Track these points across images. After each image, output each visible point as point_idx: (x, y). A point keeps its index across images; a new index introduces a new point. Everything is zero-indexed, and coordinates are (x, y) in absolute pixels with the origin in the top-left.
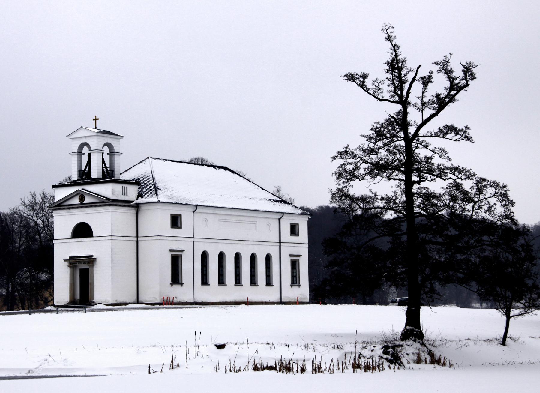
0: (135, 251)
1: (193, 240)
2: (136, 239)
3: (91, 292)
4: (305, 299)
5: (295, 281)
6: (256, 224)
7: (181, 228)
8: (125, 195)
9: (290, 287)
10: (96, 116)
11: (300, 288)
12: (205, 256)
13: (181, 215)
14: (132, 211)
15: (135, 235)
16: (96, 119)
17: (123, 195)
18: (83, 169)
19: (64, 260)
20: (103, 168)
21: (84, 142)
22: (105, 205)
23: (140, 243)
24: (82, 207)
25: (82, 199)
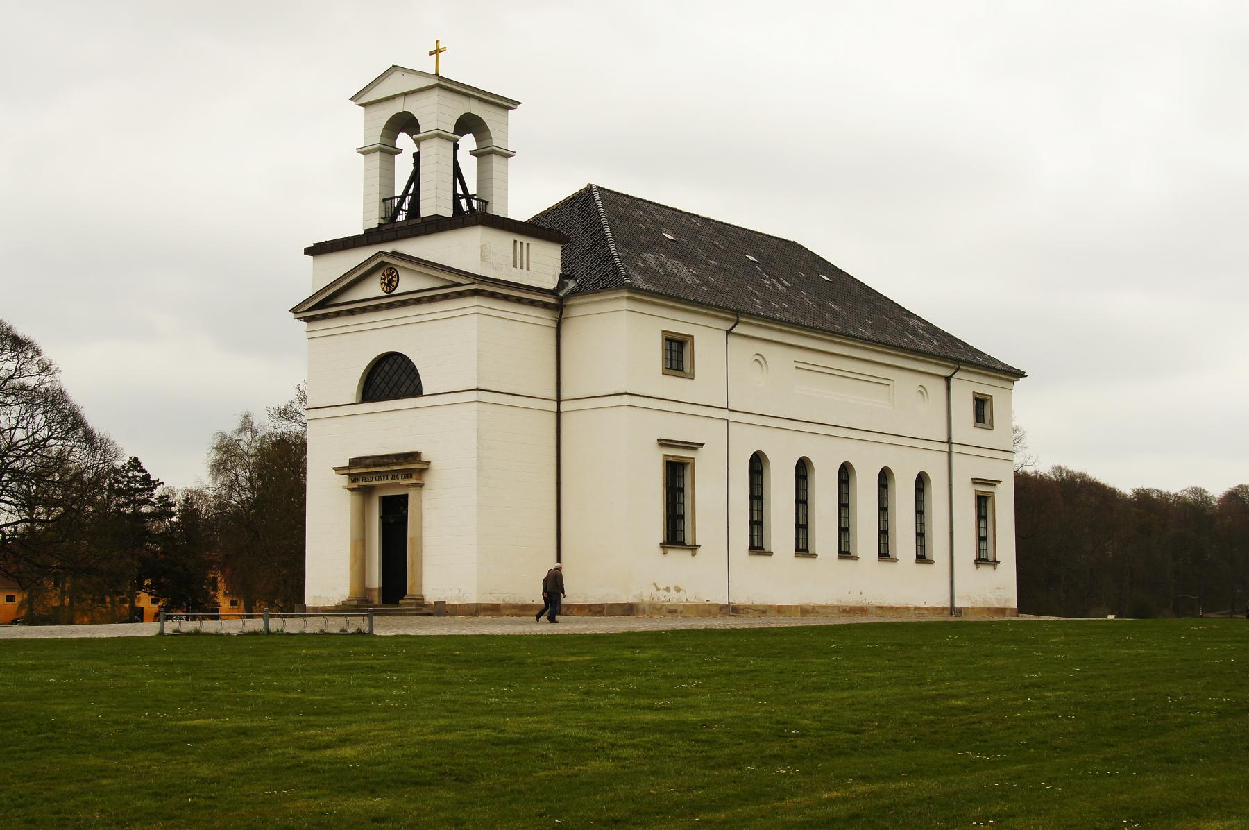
1: (725, 414)
2: (554, 406)
4: (1007, 600)
5: (984, 559)
7: (691, 376)
8: (522, 268)
11: (996, 570)
12: (757, 464)
13: (692, 337)
14: (540, 320)
15: (553, 395)
16: (437, 52)
17: (515, 266)
18: (399, 191)
20: (455, 194)
22: (461, 295)
23: (563, 416)
24: (390, 306)
25: (390, 284)
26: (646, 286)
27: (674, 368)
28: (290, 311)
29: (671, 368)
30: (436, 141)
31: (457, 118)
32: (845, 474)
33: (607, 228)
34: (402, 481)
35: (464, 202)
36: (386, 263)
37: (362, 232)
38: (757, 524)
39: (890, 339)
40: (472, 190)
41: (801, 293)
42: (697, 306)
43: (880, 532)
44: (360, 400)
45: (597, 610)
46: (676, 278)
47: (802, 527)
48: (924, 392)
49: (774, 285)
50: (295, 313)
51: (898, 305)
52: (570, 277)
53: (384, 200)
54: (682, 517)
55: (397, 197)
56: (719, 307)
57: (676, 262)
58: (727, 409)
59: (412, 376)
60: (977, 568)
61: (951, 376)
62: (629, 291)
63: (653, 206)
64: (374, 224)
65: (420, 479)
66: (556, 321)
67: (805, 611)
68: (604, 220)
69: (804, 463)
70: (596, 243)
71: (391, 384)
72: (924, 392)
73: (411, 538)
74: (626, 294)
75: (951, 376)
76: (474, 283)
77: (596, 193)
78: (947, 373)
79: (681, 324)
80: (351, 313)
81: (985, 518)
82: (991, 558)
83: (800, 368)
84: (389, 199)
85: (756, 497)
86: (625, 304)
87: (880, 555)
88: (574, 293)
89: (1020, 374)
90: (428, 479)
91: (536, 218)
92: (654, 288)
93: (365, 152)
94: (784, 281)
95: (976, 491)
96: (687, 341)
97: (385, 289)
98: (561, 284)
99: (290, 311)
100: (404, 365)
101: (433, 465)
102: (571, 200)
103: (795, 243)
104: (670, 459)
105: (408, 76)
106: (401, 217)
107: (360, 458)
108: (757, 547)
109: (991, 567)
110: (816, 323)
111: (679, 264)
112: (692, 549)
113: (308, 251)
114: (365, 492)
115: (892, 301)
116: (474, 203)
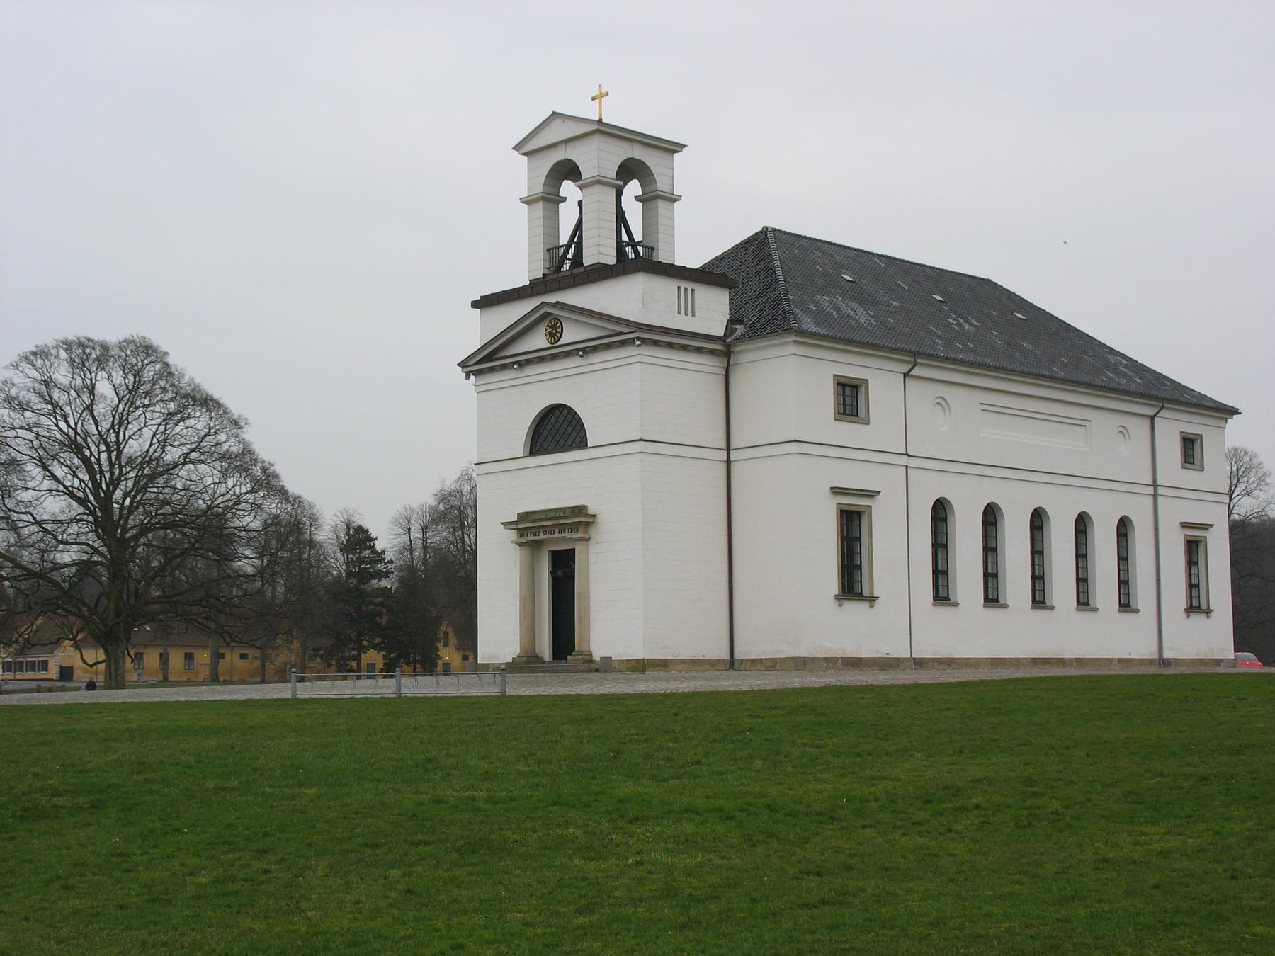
0: (723, 405)
1: (904, 460)
2: (723, 455)
3: (580, 620)
5: (1196, 606)
6: (1088, 426)
7: (866, 422)
8: (686, 314)
9: (1184, 615)
10: (600, 86)
12: (941, 512)
13: (867, 381)
17: (680, 313)
18: (564, 239)
19: (502, 523)
21: (563, 158)
22: (623, 343)
23: (734, 467)
24: (554, 357)
25: (555, 333)
26: (815, 329)
27: (847, 413)
28: (458, 365)
29: (845, 413)
30: (597, 188)
31: (619, 164)
32: (1082, 524)
33: (779, 271)
34: (568, 535)
35: (629, 250)
36: (550, 314)
37: (527, 283)
38: (941, 575)
39: (1086, 379)
40: (638, 237)
41: (991, 333)
42: (872, 349)
43: (1120, 582)
44: (528, 454)
45: (770, 665)
46: (851, 321)
47: (1083, 581)
48: (1124, 431)
49: (960, 325)
50: (463, 367)
51: (1100, 342)
52: (741, 322)
53: (549, 250)
54: (860, 567)
55: (563, 246)
56: (895, 349)
57: (853, 304)
58: (907, 454)
59: (578, 428)
60: (1188, 617)
61: (1155, 415)
62: (796, 335)
63: (833, 247)
64: (539, 274)
65: (587, 533)
66: (724, 368)
67: (996, 662)
68: (777, 263)
69: (1039, 513)
70: (767, 287)
71: (558, 437)
72: (1124, 431)
73: (579, 593)
74: (794, 338)
75: (1155, 415)
76: (636, 332)
77: (770, 236)
78: (1151, 412)
79: (853, 367)
80: (522, 365)
81: (1197, 563)
82: (1204, 606)
83: (985, 410)
84: (553, 249)
85: (940, 545)
86: (793, 349)
87: (986, 599)
88: (741, 339)
89: (1234, 412)
90: (593, 533)
91: (711, 263)
92: (824, 331)
93: (528, 202)
94: (973, 321)
95: (1185, 535)
96: (861, 386)
97: (550, 340)
98: (729, 330)
99: (458, 365)
100: (570, 417)
101: (599, 518)
102: (746, 243)
103: (989, 280)
104: (844, 508)
105: (567, 123)
106: (566, 267)
107: (527, 513)
108: (942, 595)
109: (1204, 616)
110: (1003, 364)
111: (856, 306)
112: (870, 601)
113: (475, 304)
114: (533, 547)
115: (1093, 338)
116: (641, 249)
